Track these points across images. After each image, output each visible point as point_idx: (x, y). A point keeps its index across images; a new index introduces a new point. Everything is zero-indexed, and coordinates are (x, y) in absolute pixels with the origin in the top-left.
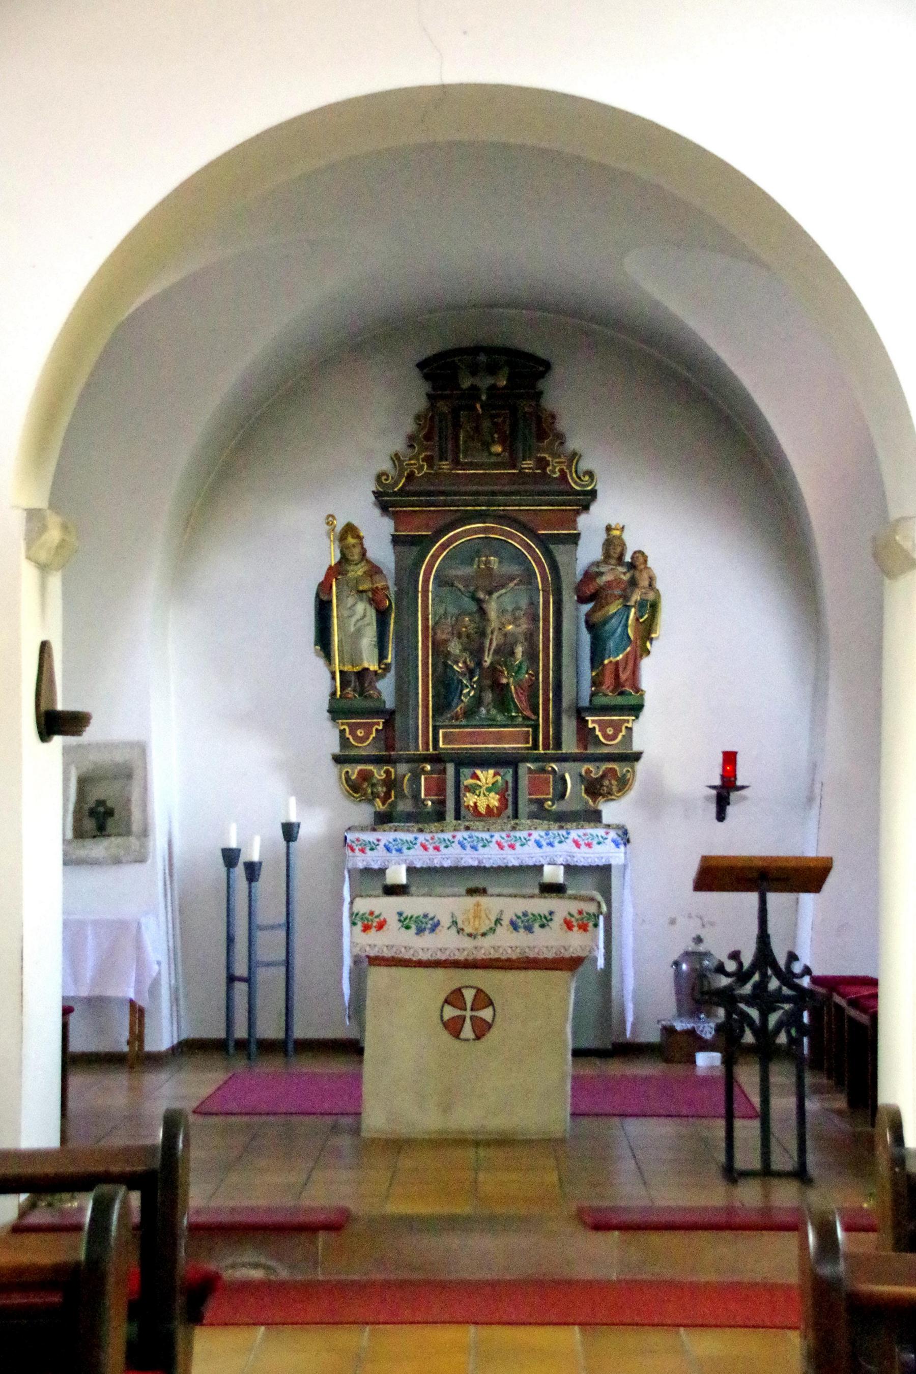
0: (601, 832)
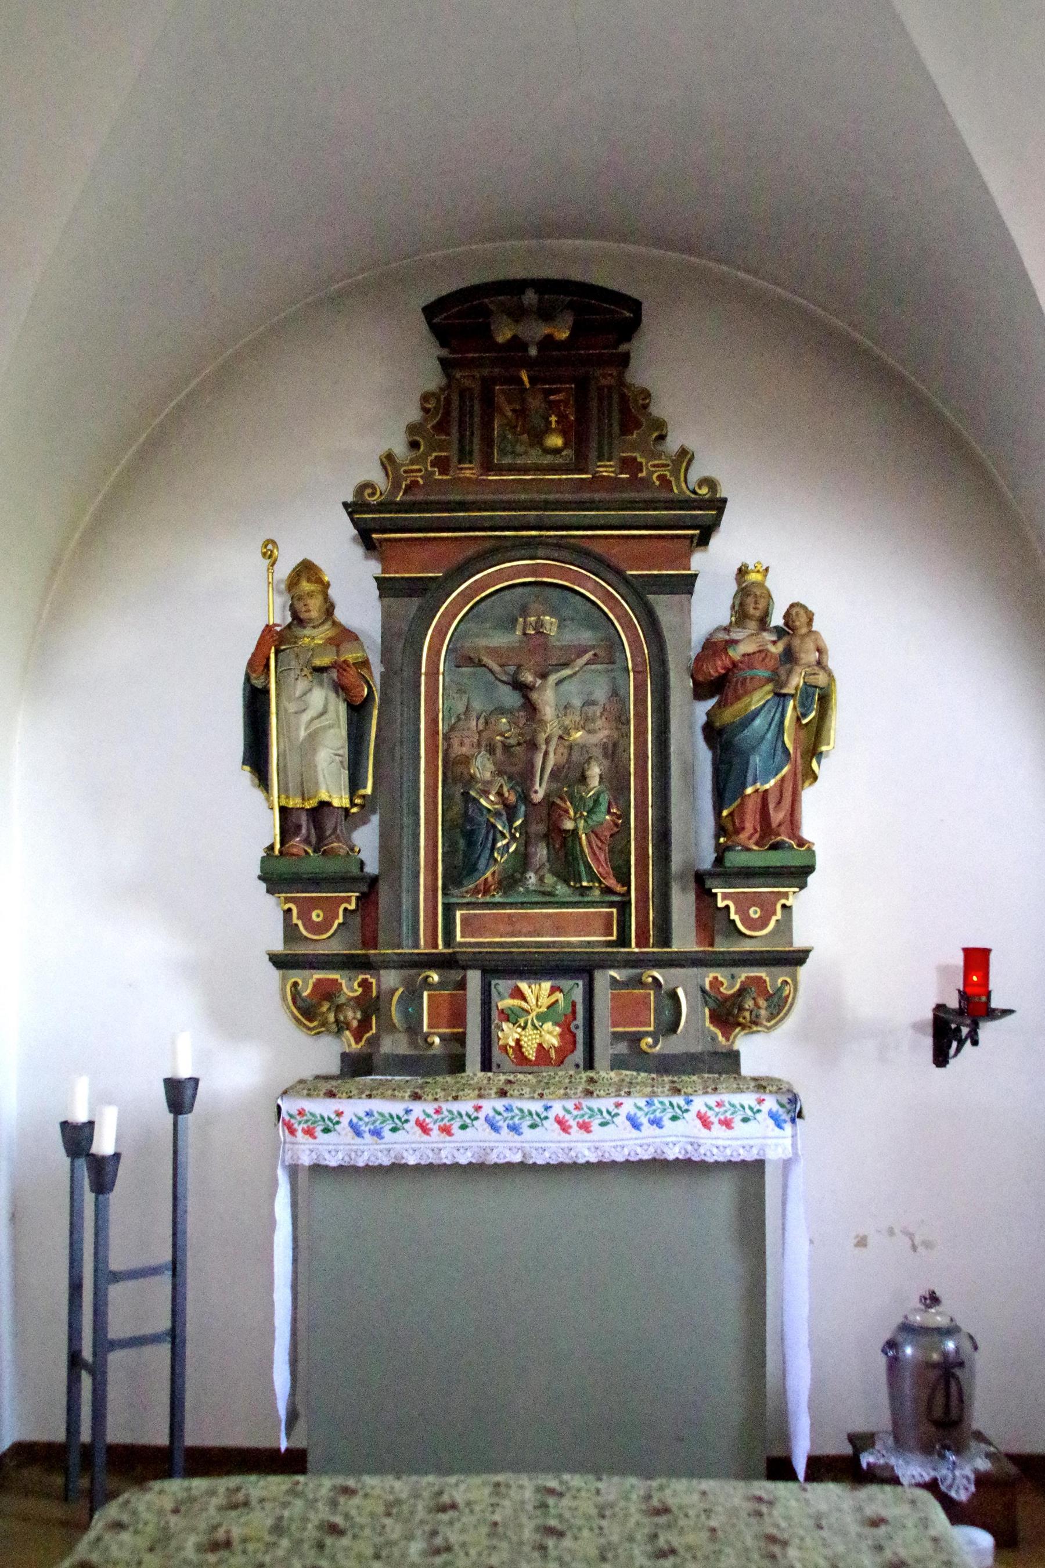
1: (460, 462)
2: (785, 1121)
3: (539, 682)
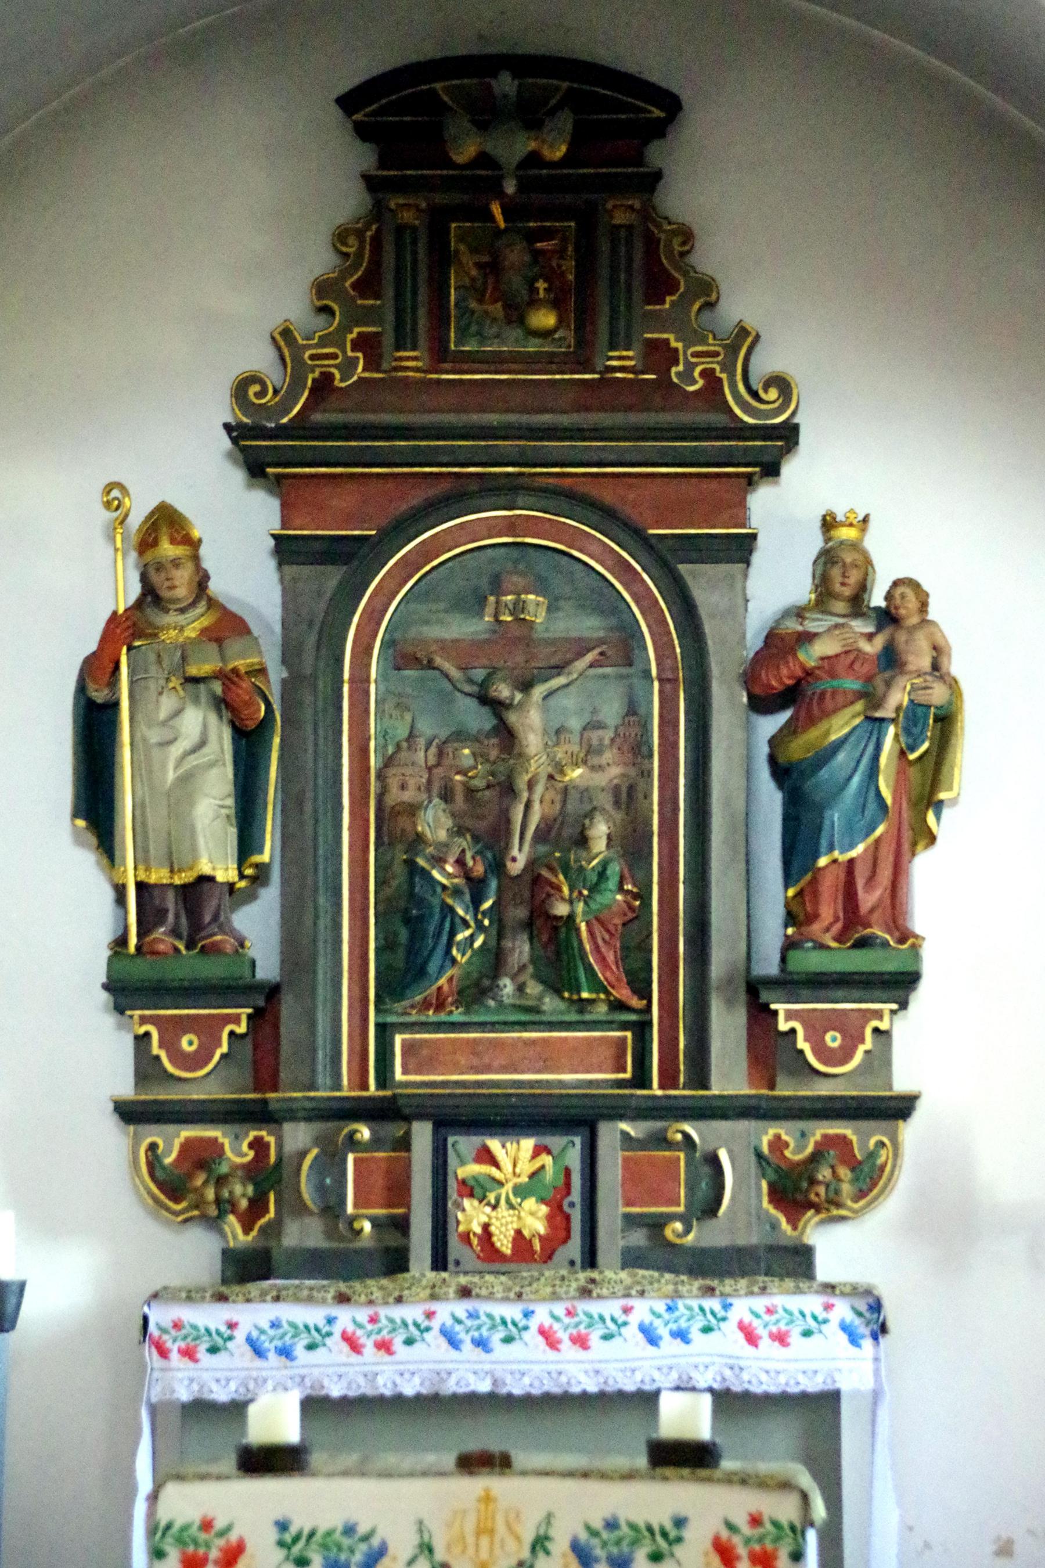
0: (812, 1303)
1: (398, 348)
2: (863, 1337)
3: (518, 696)
